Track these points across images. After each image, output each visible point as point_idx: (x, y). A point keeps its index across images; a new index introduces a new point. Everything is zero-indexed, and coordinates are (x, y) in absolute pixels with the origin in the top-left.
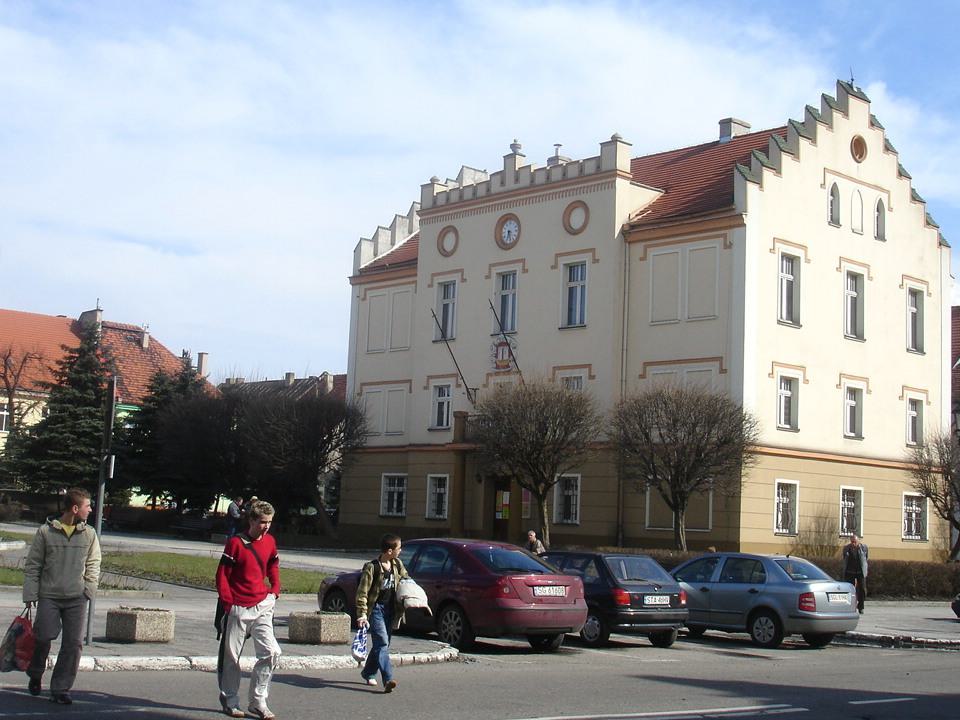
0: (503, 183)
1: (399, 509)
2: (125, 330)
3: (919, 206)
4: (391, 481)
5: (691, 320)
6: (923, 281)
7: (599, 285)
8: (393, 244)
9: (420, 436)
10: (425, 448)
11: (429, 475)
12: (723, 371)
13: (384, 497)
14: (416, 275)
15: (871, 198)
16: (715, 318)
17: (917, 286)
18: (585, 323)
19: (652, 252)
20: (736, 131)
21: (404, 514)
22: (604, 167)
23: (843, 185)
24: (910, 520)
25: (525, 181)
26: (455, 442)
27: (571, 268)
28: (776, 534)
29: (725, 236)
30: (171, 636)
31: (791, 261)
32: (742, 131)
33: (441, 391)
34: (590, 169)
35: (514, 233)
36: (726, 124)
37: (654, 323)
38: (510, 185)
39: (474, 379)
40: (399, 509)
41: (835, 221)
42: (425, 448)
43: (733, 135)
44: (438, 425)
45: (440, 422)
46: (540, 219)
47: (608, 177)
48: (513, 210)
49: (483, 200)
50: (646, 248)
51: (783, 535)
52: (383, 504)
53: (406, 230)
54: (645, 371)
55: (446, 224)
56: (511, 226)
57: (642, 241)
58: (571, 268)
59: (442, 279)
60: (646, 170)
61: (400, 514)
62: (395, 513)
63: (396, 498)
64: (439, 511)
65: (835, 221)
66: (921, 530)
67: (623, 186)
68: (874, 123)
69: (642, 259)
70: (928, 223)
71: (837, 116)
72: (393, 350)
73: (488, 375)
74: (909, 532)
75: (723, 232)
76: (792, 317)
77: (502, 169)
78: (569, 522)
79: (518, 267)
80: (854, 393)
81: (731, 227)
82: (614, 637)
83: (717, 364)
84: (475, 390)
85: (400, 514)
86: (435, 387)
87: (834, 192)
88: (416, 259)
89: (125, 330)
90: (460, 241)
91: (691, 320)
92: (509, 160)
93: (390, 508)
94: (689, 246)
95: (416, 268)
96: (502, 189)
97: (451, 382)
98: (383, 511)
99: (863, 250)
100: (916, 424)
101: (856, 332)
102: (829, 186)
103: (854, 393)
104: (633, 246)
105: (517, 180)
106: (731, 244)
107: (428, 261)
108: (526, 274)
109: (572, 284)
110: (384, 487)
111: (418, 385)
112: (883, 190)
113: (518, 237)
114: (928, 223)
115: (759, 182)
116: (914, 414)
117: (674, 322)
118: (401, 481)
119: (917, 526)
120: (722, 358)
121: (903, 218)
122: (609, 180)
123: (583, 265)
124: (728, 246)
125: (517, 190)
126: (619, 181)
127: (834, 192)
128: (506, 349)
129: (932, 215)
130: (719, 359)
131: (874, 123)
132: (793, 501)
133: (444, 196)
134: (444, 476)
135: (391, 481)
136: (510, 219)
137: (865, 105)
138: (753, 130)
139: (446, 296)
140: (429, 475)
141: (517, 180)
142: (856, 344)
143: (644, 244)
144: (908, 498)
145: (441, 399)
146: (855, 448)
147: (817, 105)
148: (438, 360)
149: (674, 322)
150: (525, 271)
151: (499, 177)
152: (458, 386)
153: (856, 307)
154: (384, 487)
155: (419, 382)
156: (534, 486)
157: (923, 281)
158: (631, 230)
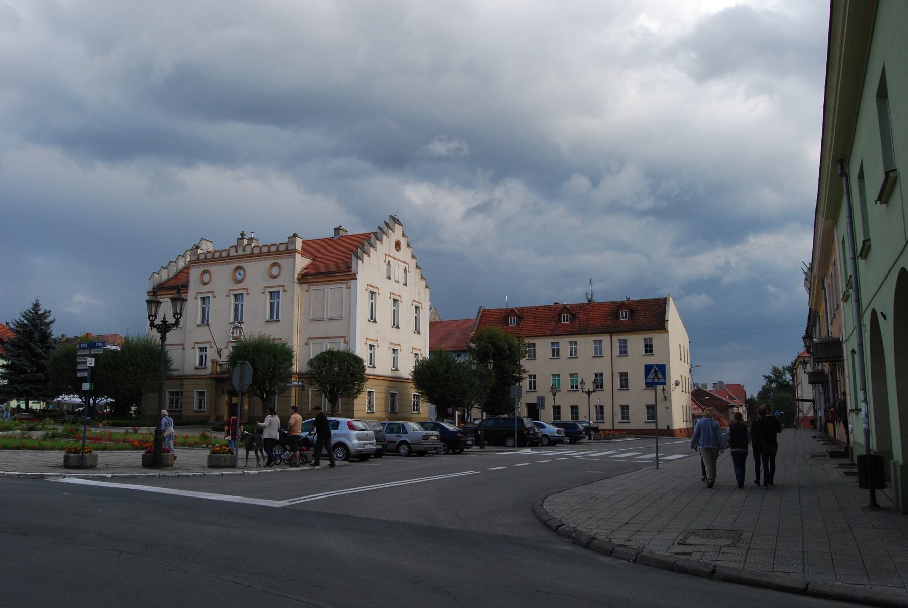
0: (236, 252)
1: (176, 407)
3: (419, 270)
4: (172, 393)
5: (331, 320)
6: (420, 303)
9: (189, 370)
12: (345, 342)
14: (187, 293)
15: (402, 266)
18: (280, 318)
19: (312, 288)
20: (342, 233)
21: (179, 409)
23: (392, 260)
26: (211, 374)
28: (367, 413)
32: (344, 234)
33: (201, 349)
36: (337, 230)
38: (240, 252)
40: (176, 407)
43: (341, 235)
44: (625, 341)
45: (201, 364)
47: (292, 253)
48: (278, 261)
50: (309, 286)
55: (205, 269)
58: (271, 293)
59: (203, 295)
60: (310, 248)
61: (177, 409)
62: (174, 409)
63: (174, 401)
67: (298, 257)
69: (307, 291)
73: (229, 342)
76: (373, 320)
79: (211, 295)
82: (411, 454)
83: (181, 346)
84: (221, 349)
85: (177, 409)
88: (188, 285)
91: (331, 320)
99: (398, 289)
102: (387, 262)
108: (285, 293)
109: (204, 306)
111: (188, 346)
112: (406, 264)
113: (244, 277)
118: (177, 393)
120: (345, 336)
123: (209, 297)
124: (349, 288)
130: (344, 337)
131: (403, 235)
135: (172, 393)
137: (401, 227)
138: (348, 233)
140: (195, 390)
141: (244, 251)
152: (211, 347)
155: (188, 345)
156: (260, 395)
157: (420, 303)
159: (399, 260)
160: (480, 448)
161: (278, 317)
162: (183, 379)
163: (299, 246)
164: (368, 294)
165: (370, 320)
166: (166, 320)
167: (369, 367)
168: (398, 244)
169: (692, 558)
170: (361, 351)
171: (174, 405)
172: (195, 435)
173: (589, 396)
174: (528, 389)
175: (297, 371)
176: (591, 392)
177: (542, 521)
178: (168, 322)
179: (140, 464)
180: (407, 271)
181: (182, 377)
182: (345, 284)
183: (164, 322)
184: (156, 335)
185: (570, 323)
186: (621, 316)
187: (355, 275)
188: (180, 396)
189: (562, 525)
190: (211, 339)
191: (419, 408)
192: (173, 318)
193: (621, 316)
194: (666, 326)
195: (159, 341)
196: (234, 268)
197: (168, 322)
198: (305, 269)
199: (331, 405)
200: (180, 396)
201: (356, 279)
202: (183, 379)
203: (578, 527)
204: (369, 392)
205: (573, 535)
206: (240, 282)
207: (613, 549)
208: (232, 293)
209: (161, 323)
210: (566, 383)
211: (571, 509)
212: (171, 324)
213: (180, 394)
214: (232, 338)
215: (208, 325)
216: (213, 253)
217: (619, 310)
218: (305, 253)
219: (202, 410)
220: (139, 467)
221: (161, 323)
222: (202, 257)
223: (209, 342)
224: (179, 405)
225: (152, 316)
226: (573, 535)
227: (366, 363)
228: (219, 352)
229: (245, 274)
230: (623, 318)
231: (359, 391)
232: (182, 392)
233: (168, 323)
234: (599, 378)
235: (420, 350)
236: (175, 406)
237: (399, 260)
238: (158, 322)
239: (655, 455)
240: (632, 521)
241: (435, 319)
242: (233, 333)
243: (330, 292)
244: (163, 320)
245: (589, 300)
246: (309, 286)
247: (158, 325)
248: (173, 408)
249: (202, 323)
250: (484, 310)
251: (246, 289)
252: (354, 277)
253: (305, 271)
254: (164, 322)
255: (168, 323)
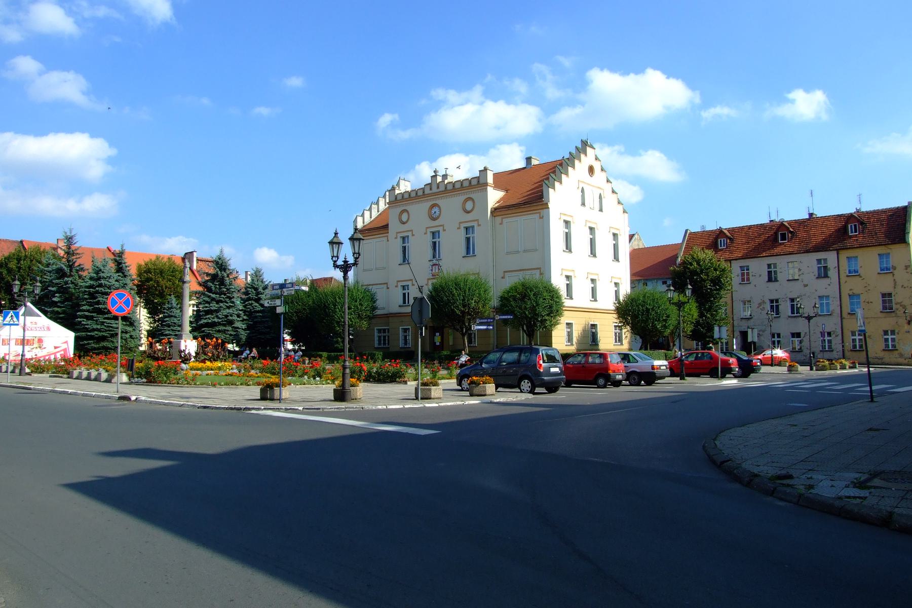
1: (384, 344)
2: (207, 261)
4: (379, 331)
5: (525, 251)
7: (478, 237)
8: (371, 217)
9: (395, 309)
10: (397, 315)
11: (400, 328)
13: (376, 339)
16: (536, 250)
17: (616, 232)
18: (476, 254)
19: (505, 221)
21: (387, 346)
22: (482, 181)
24: (616, 336)
25: (442, 188)
27: (467, 229)
28: (566, 345)
29: (540, 213)
30: (442, 396)
31: (567, 223)
33: (404, 287)
34: (474, 182)
35: (438, 213)
37: (508, 253)
38: (435, 190)
39: (422, 281)
40: (384, 344)
41: (583, 204)
42: (397, 315)
45: (404, 302)
46: (451, 206)
48: (471, 196)
49: (458, 190)
50: (502, 219)
51: (568, 345)
52: (376, 342)
53: (376, 211)
54: (504, 275)
56: (436, 209)
57: (501, 215)
58: (467, 229)
61: (385, 346)
64: (406, 343)
65: (583, 204)
66: (620, 340)
67: (490, 190)
68: (597, 159)
70: (619, 203)
71: (582, 156)
72: (377, 269)
73: (428, 279)
74: (616, 342)
75: (539, 211)
76: (568, 247)
77: (430, 182)
78: (472, 345)
80: (593, 281)
81: (542, 209)
83: (386, 285)
86: (401, 286)
87: (583, 190)
88: (388, 225)
89: (207, 261)
90: (410, 216)
91: (525, 251)
92: (434, 178)
93: (380, 343)
94: (525, 217)
95: (388, 229)
96: (431, 192)
97: (409, 283)
98: (376, 346)
99: (594, 217)
100: (617, 293)
101: (593, 253)
103: (593, 281)
104: (496, 217)
105: (438, 188)
106: (543, 217)
107: (394, 227)
110: (376, 334)
113: (440, 215)
114: (619, 203)
115: (554, 188)
116: (593, 285)
117: (518, 252)
118: (384, 331)
119: (619, 339)
121: (610, 201)
122: (484, 187)
124: (541, 218)
125: (431, 194)
126: (488, 188)
127: (583, 190)
128: (437, 267)
129: (620, 199)
131: (597, 159)
132: (572, 331)
133: (401, 195)
134: (407, 327)
135: (379, 331)
136: (435, 206)
137: (593, 150)
139: (404, 243)
140: (400, 328)
142: (593, 259)
143: (501, 217)
144: (615, 326)
145: (404, 292)
146: (594, 305)
147: (574, 151)
148: (404, 273)
149: (518, 252)
150: (444, 230)
151: (429, 186)
152: (413, 285)
153: (592, 242)
154: (376, 334)
155: (392, 284)
158: (495, 210)
159: (593, 186)
160: (681, 379)
161: (474, 253)
162: (388, 317)
163: (490, 179)
164: (563, 224)
165: (565, 250)
166: (347, 260)
167: (565, 298)
168: (591, 170)
169: (865, 503)
170: (558, 281)
171: (382, 343)
172: (657, 363)
173: (809, 322)
174: (790, 314)
175: (495, 306)
176: (812, 317)
177: (709, 456)
178: (348, 262)
179: (333, 399)
180: (603, 197)
181: (388, 315)
182: (538, 215)
183: (345, 262)
184: (338, 275)
185: (788, 242)
186: (850, 230)
187: (547, 204)
188: (387, 333)
189: (728, 461)
190: (413, 278)
191: (572, 339)
192: (332, 260)
193: (850, 230)
194: (907, 239)
195: (342, 280)
196: (430, 205)
197: (348, 262)
198: (498, 202)
199: (528, 339)
200: (387, 333)
201: (549, 208)
202: (388, 317)
203: (744, 463)
204: (568, 324)
205: (735, 471)
206: (437, 219)
207: (775, 489)
208: (429, 230)
209: (343, 263)
210: (785, 308)
211: (746, 444)
212: (351, 264)
213: (387, 331)
214: (431, 275)
215: (409, 263)
216: (409, 193)
217: (847, 223)
218: (497, 185)
219: (408, 346)
220: (331, 401)
221: (343, 263)
222: (399, 198)
223: (412, 280)
224: (387, 342)
225: (335, 258)
226: (735, 471)
227: (563, 292)
228: (420, 289)
229: (440, 211)
230: (852, 232)
231: (557, 323)
232: (388, 329)
233: (349, 263)
234: (775, 304)
235: (620, 278)
236: (383, 343)
237: (593, 186)
238: (340, 262)
239: (874, 388)
240: (810, 459)
241: (638, 245)
242: (432, 270)
243: (523, 221)
244: (344, 260)
245: (811, 215)
246: (502, 219)
247: (340, 265)
248: (385, 345)
249: (467, 254)
250: (691, 233)
251: (443, 226)
252: (546, 206)
253: (498, 204)
254: (345, 262)
255: (349, 263)
